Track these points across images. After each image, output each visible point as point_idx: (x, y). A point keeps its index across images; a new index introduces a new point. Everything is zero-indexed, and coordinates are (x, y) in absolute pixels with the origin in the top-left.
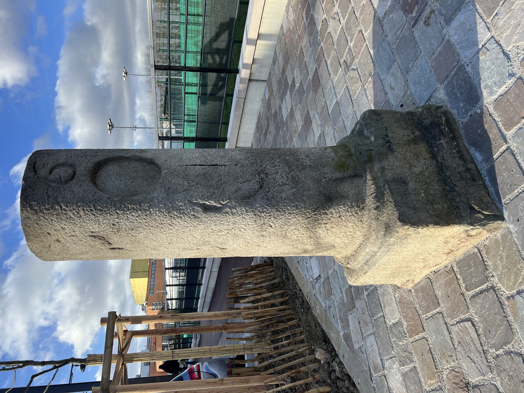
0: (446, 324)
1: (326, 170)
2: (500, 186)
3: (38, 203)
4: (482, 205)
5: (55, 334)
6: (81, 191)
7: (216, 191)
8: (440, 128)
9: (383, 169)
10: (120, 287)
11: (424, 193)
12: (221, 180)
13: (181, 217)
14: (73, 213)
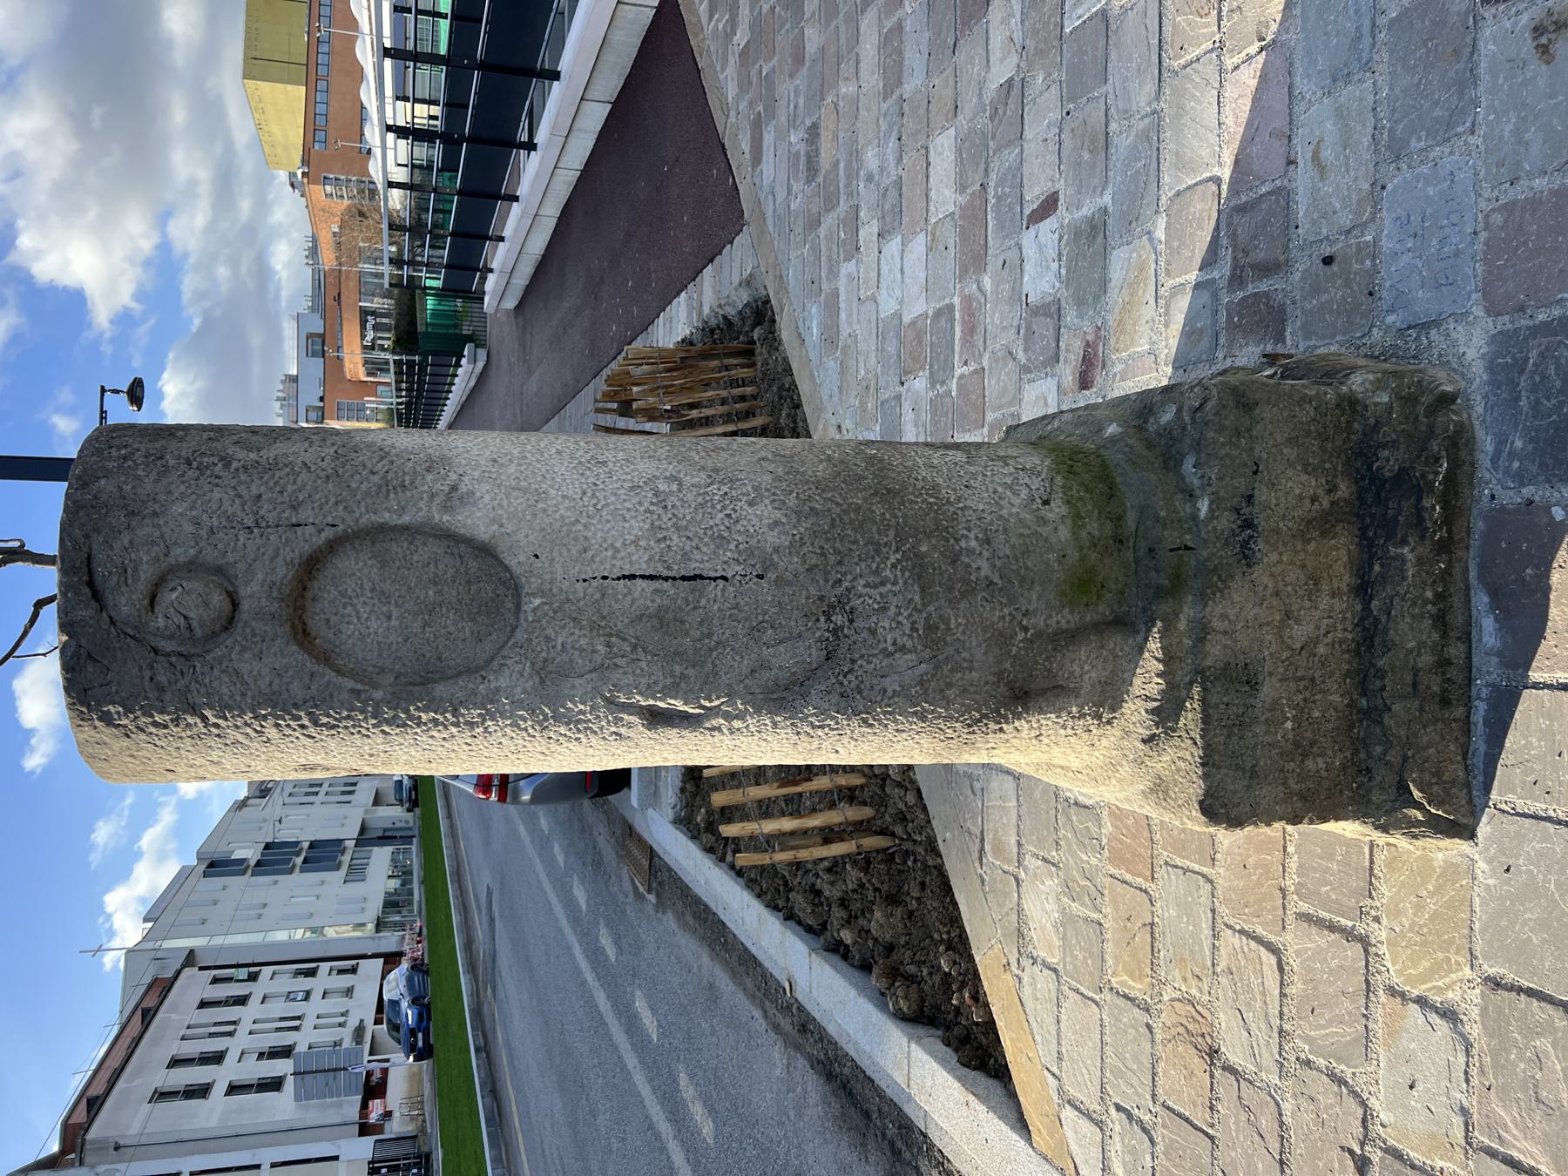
0: (1213, 911)
1: (1033, 599)
2: (1506, 758)
4: (1435, 788)
5: (12, 258)
6: (265, 671)
7: (690, 672)
8: (1419, 499)
9: (1202, 632)
10: (209, 114)
11: (1294, 718)
12: (710, 635)
13: (577, 739)
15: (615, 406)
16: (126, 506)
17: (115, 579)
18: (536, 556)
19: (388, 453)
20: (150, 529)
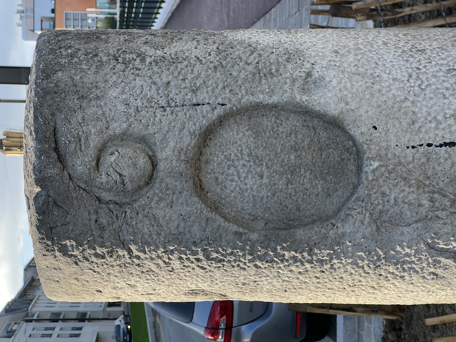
3: (79, 244)
6: (174, 217)
13: (402, 277)
14: (158, 265)
15: (327, 7)
16: (78, 91)
17: (73, 146)
18: (375, 128)
19: (255, 48)
20: (94, 109)
